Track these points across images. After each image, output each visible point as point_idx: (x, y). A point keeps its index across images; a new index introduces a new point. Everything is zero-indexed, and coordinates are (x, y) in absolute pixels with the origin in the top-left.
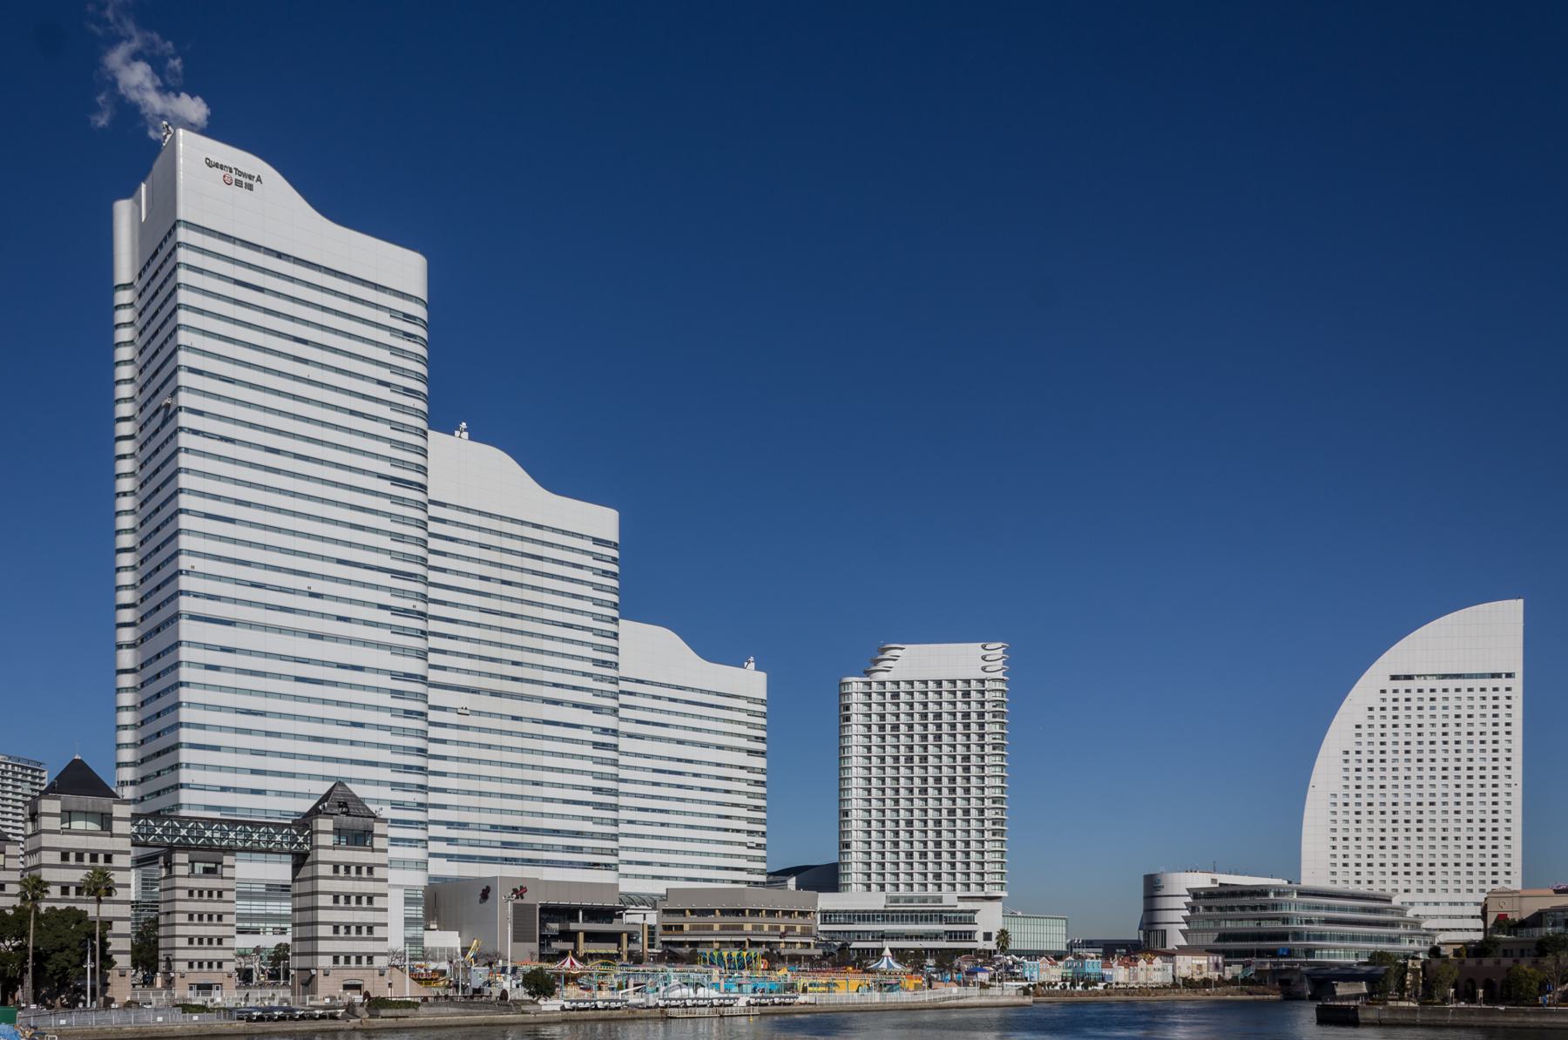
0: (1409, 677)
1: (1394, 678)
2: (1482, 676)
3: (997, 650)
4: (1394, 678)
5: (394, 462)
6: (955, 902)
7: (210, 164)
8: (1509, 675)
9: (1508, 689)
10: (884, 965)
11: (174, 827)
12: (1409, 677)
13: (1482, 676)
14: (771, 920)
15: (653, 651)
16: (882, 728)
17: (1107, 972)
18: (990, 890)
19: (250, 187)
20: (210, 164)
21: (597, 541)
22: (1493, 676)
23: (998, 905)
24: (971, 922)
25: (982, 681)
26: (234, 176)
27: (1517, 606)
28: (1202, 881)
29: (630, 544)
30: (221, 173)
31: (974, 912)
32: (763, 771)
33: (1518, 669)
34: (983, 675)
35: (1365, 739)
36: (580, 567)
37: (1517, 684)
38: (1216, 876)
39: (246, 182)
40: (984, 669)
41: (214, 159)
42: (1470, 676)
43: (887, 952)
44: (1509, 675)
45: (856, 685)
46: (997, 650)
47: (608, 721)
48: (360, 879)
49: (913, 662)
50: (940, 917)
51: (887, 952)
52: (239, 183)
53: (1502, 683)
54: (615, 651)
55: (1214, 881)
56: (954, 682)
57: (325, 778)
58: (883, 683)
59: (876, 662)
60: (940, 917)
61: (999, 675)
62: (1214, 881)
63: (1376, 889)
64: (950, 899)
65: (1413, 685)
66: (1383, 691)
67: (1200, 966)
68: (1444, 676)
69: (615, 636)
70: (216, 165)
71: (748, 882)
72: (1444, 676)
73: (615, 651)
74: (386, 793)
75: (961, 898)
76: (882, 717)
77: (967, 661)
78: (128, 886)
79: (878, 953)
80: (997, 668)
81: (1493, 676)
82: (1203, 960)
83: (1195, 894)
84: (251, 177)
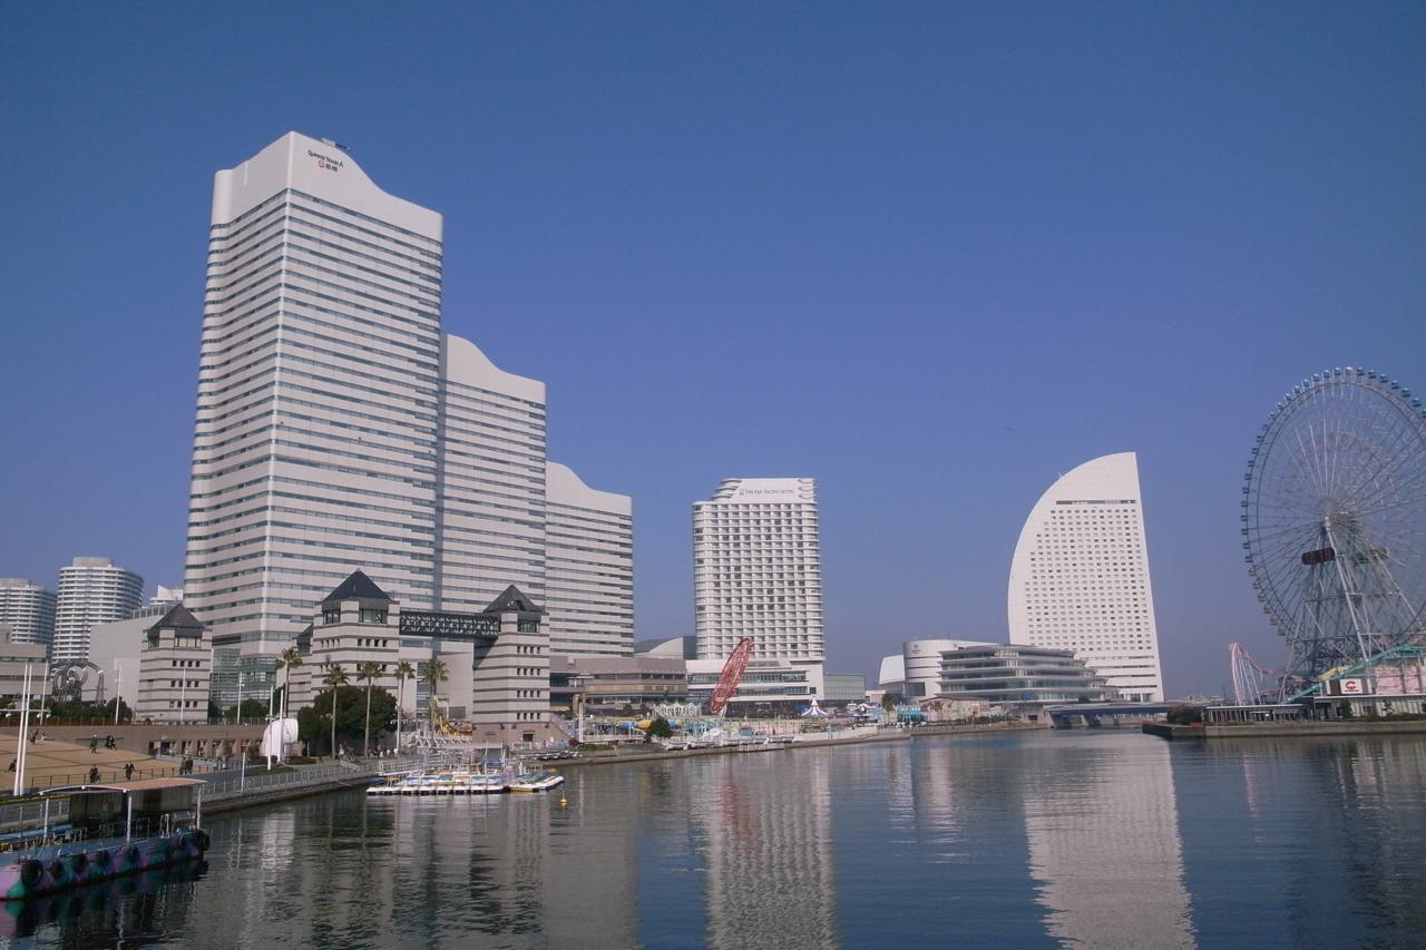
0: (1070, 503)
1: (1059, 503)
2: (1116, 502)
3: (808, 483)
4: (1059, 503)
5: (420, 351)
6: (790, 665)
7: (311, 154)
8: (1132, 502)
9: (1133, 511)
10: (814, 713)
11: (446, 622)
12: (1070, 503)
13: (1116, 502)
14: (668, 682)
15: (564, 484)
16: (737, 537)
17: (924, 714)
18: (812, 657)
19: (335, 169)
20: (311, 154)
21: (531, 404)
22: (1123, 502)
23: (820, 666)
24: (803, 679)
25: (799, 505)
26: (326, 162)
27: (1134, 454)
28: (948, 646)
29: (548, 413)
30: (318, 160)
31: (804, 672)
32: (630, 569)
33: (1137, 496)
34: (799, 501)
35: (1044, 544)
36: (404, 424)
37: (1138, 507)
38: (956, 642)
39: (333, 166)
40: (801, 496)
41: (314, 151)
42: (1109, 502)
43: (814, 703)
44: (1132, 502)
45: (706, 506)
46: (808, 483)
47: (539, 534)
48: (533, 656)
49: (752, 491)
50: (779, 677)
51: (814, 703)
52: (328, 166)
53: (1129, 506)
54: (543, 482)
55: (955, 645)
56: (778, 505)
57: (334, 575)
58: (726, 506)
59: (718, 491)
60: (779, 677)
61: (812, 501)
62: (955, 645)
63: (1062, 648)
64: (784, 663)
65: (1072, 507)
66: (1053, 512)
67: (976, 708)
68: (1092, 502)
69: (543, 471)
70: (315, 155)
71: (622, 653)
72: (1092, 502)
73: (543, 482)
74: (407, 589)
75: (793, 663)
76: (737, 530)
77: (793, 491)
78: (209, 660)
79: (807, 704)
80: (809, 497)
81: (1123, 502)
82: (977, 704)
83: (946, 655)
84: (336, 163)
